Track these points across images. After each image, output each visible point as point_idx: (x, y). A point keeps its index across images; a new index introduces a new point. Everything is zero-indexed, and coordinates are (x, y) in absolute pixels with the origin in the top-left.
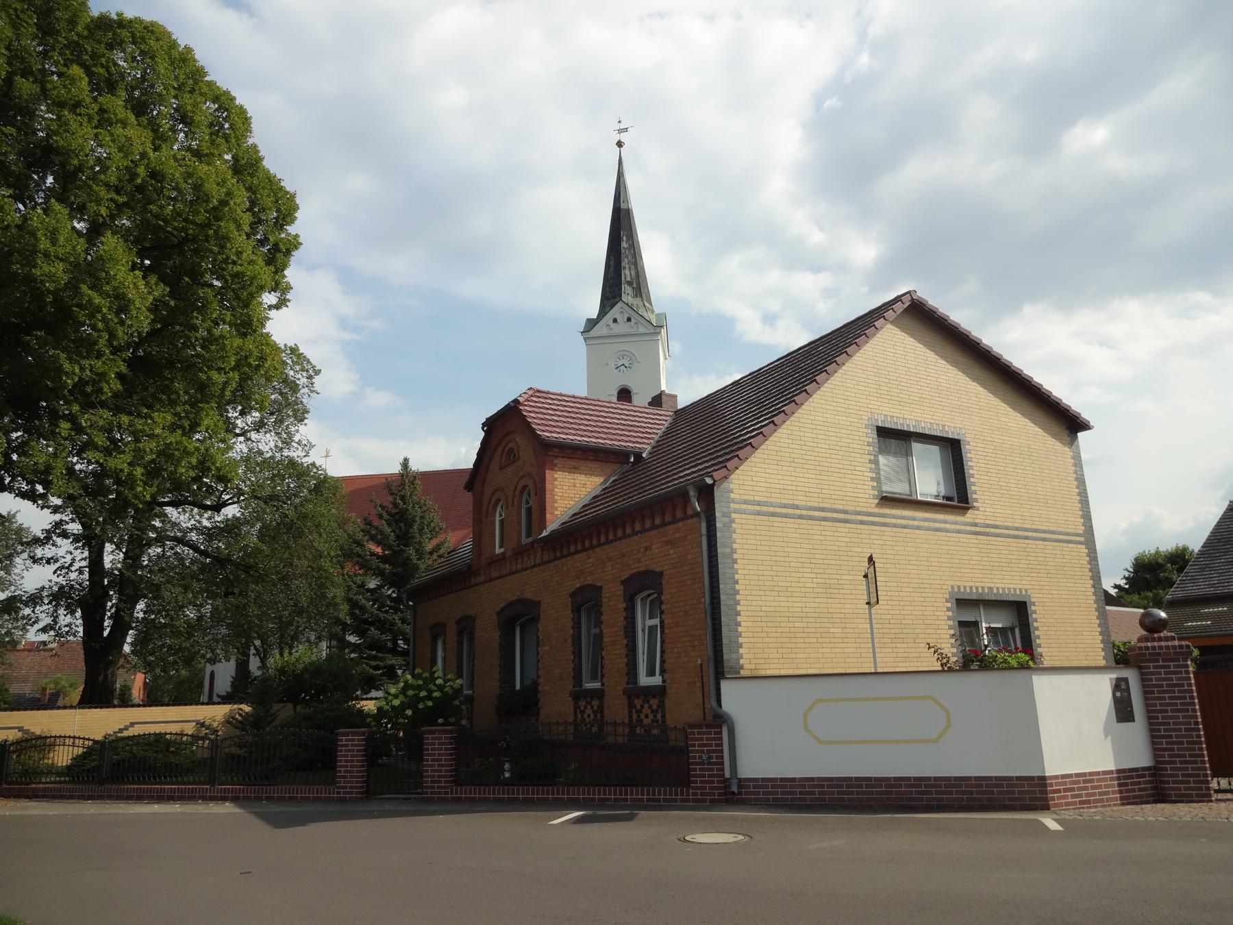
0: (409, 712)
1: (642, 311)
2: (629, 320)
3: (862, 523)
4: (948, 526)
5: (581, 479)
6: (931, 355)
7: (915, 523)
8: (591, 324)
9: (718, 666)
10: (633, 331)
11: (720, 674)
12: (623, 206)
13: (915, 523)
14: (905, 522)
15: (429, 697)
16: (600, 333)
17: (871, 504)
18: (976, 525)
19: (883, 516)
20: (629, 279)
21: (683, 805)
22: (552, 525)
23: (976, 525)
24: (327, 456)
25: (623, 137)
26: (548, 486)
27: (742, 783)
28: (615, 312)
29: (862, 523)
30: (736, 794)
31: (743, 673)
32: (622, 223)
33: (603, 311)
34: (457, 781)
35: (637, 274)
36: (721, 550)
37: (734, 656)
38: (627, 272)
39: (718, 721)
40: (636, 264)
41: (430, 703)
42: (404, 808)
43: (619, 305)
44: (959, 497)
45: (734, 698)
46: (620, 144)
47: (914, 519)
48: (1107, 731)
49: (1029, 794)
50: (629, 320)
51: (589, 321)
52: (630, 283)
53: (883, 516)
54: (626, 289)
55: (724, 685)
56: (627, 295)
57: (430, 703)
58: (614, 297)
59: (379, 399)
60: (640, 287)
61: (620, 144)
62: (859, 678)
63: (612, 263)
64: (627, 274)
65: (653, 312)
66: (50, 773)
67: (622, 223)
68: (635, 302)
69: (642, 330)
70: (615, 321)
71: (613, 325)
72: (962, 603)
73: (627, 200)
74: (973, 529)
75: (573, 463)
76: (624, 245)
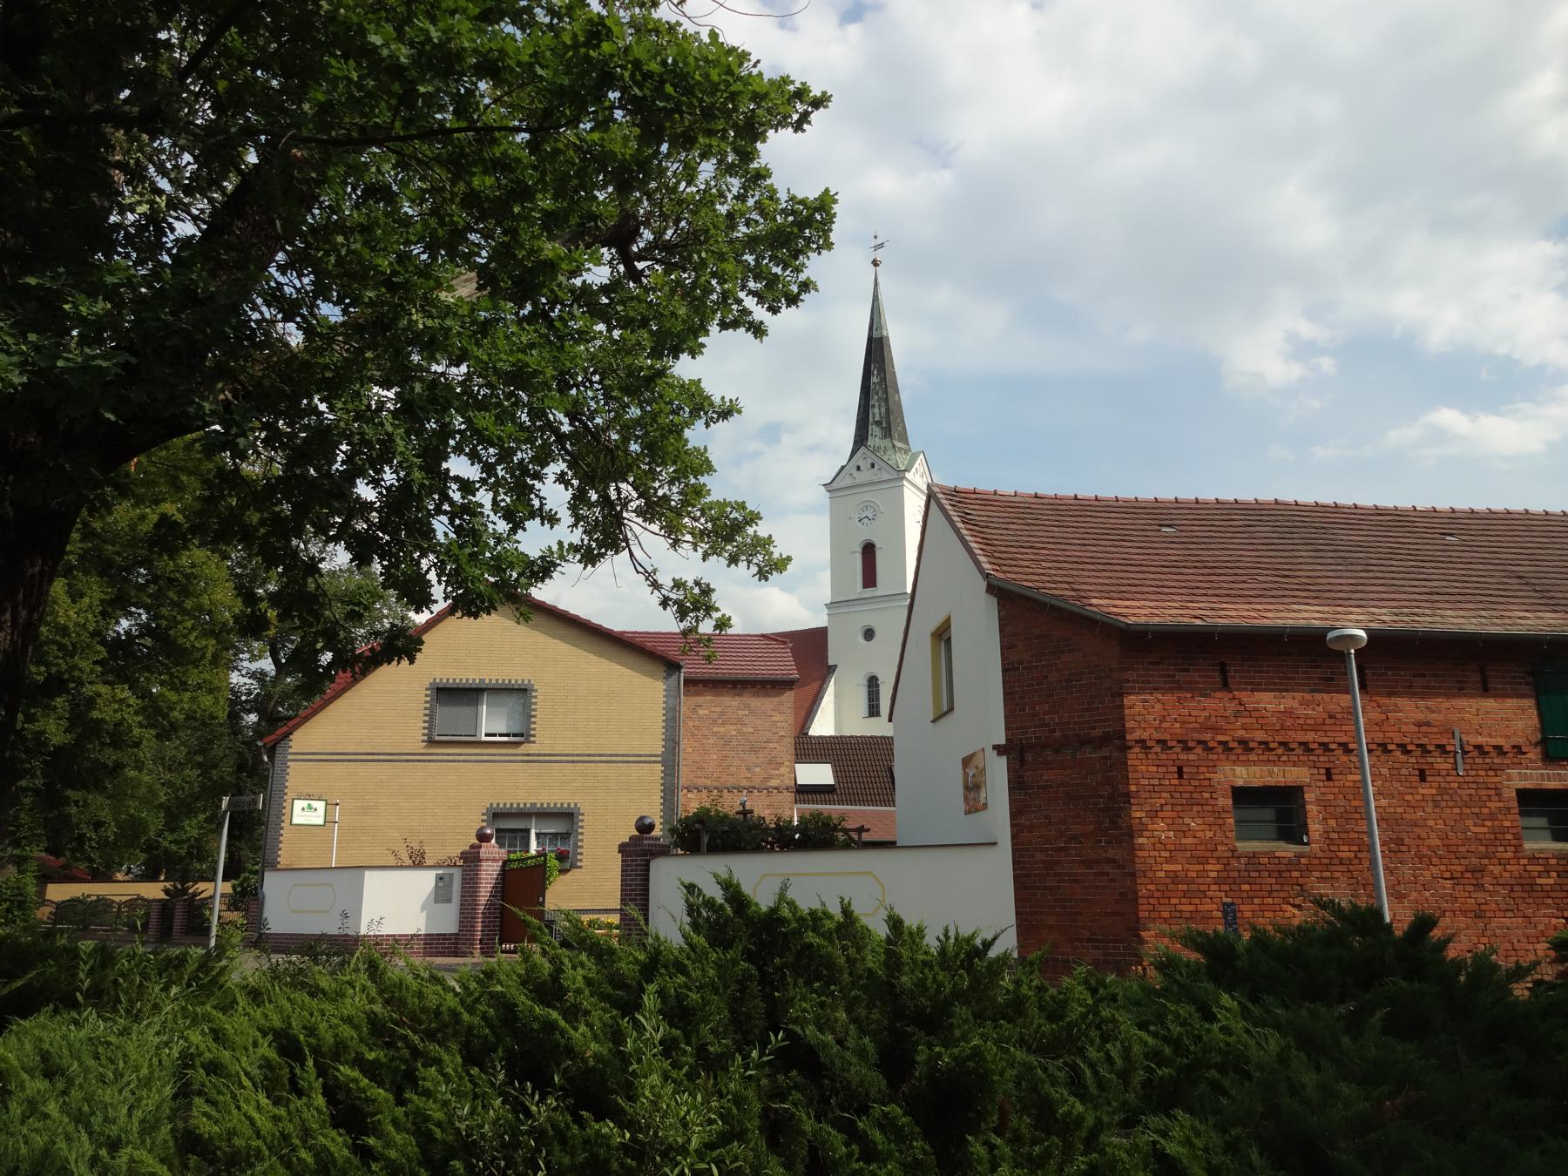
2: (873, 466)
10: (875, 479)
16: (842, 485)
17: (420, 747)
32: (877, 351)
34: (187, 933)
35: (888, 410)
38: (876, 411)
40: (886, 400)
44: (522, 736)
50: (873, 466)
52: (878, 423)
54: (874, 430)
61: (875, 263)
64: (876, 413)
67: (877, 351)
68: (886, 443)
69: (886, 476)
70: (858, 468)
73: (880, 328)
76: (874, 379)
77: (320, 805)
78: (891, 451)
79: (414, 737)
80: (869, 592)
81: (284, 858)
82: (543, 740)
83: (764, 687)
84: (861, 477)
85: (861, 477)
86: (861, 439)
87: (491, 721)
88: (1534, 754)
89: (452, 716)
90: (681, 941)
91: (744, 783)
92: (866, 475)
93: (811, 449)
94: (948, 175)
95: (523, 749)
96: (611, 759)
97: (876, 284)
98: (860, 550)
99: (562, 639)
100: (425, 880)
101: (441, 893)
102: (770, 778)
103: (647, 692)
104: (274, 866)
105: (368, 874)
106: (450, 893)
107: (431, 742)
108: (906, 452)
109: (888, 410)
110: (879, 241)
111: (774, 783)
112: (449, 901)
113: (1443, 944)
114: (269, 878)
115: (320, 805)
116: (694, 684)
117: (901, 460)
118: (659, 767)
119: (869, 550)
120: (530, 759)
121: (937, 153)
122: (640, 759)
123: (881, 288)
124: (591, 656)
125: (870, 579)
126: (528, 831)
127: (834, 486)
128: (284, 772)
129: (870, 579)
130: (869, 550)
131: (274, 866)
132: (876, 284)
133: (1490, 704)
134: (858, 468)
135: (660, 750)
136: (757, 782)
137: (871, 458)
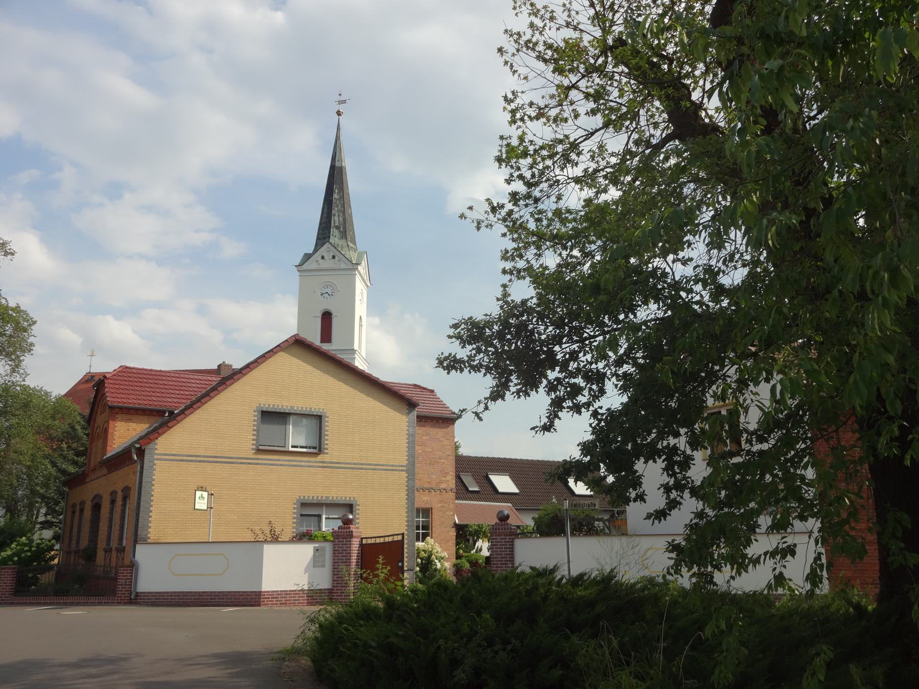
0: (16, 559)
2: (334, 257)
3: (242, 463)
4: (303, 464)
5: (133, 425)
6: (309, 368)
7: (279, 463)
8: (307, 257)
9: (136, 539)
10: (336, 267)
11: (136, 542)
13: (279, 463)
14: (272, 462)
15: (30, 551)
17: (250, 453)
18: (324, 462)
19: (258, 459)
20: (337, 224)
23: (324, 462)
24: (92, 356)
25: (342, 108)
26: (110, 430)
27: (137, 594)
28: (323, 251)
29: (242, 463)
30: (137, 600)
31: (149, 541)
32: (336, 176)
33: (316, 250)
34: (15, 595)
35: (344, 219)
36: (144, 479)
37: (144, 533)
38: (336, 218)
39: (133, 566)
40: (344, 212)
41: (29, 554)
43: (327, 245)
44: (318, 449)
45: (142, 554)
46: (339, 113)
47: (279, 460)
48: (306, 570)
49: (252, 599)
50: (334, 257)
51: (306, 254)
52: (337, 228)
53: (258, 459)
54: (334, 232)
55: (138, 547)
57: (29, 554)
58: (324, 238)
59: (231, 249)
60: (346, 231)
62: (167, 546)
63: (326, 210)
64: (336, 220)
65: (355, 250)
66: (52, 666)
67: (336, 176)
68: (342, 242)
69: (343, 266)
70: (323, 258)
71: (321, 261)
72: (304, 505)
73: (341, 160)
75: (129, 417)
76: (336, 196)
77: (198, 494)
78: (346, 249)
79: (245, 444)
81: (153, 533)
82: (334, 449)
83: (438, 422)
84: (324, 264)
85: (324, 264)
86: (323, 236)
87: (296, 436)
89: (273, 429)
90: (559, 577)
91: (426, 486)
92: (328, 263)
94: (279, 17)
95: (320, 458)
96: (376, 467)
97: (338, 129)
98: (320, 315)
99: (345, 382)
100: (307, 550)
101: (316, 561)
102: (442, 482)
103: (397, 423)
104: (145, 541)
105: (266, 546)
106: (324, 561)
108: (355, 250)
109: (344, 219)
110: (342, 98)
111: (443, 486)
112: (323, 566)
113: (326, 620)
115: (198, 494)
116: (423, 419)
117: (354, 257)
118: (404, 474)
119: (327, 317)
120: (325, 466)
122: (392, 469)
123: (342, 132)
124: (363, 396)
126: (319, 516)
127: (304, 267)
128: (152, 468)
130: (327, 317)
131: (145, 541)
132: (338, 129)
134: (323, 258)
135: (405, 463)
136: (433, 485)
137: (333, 252)
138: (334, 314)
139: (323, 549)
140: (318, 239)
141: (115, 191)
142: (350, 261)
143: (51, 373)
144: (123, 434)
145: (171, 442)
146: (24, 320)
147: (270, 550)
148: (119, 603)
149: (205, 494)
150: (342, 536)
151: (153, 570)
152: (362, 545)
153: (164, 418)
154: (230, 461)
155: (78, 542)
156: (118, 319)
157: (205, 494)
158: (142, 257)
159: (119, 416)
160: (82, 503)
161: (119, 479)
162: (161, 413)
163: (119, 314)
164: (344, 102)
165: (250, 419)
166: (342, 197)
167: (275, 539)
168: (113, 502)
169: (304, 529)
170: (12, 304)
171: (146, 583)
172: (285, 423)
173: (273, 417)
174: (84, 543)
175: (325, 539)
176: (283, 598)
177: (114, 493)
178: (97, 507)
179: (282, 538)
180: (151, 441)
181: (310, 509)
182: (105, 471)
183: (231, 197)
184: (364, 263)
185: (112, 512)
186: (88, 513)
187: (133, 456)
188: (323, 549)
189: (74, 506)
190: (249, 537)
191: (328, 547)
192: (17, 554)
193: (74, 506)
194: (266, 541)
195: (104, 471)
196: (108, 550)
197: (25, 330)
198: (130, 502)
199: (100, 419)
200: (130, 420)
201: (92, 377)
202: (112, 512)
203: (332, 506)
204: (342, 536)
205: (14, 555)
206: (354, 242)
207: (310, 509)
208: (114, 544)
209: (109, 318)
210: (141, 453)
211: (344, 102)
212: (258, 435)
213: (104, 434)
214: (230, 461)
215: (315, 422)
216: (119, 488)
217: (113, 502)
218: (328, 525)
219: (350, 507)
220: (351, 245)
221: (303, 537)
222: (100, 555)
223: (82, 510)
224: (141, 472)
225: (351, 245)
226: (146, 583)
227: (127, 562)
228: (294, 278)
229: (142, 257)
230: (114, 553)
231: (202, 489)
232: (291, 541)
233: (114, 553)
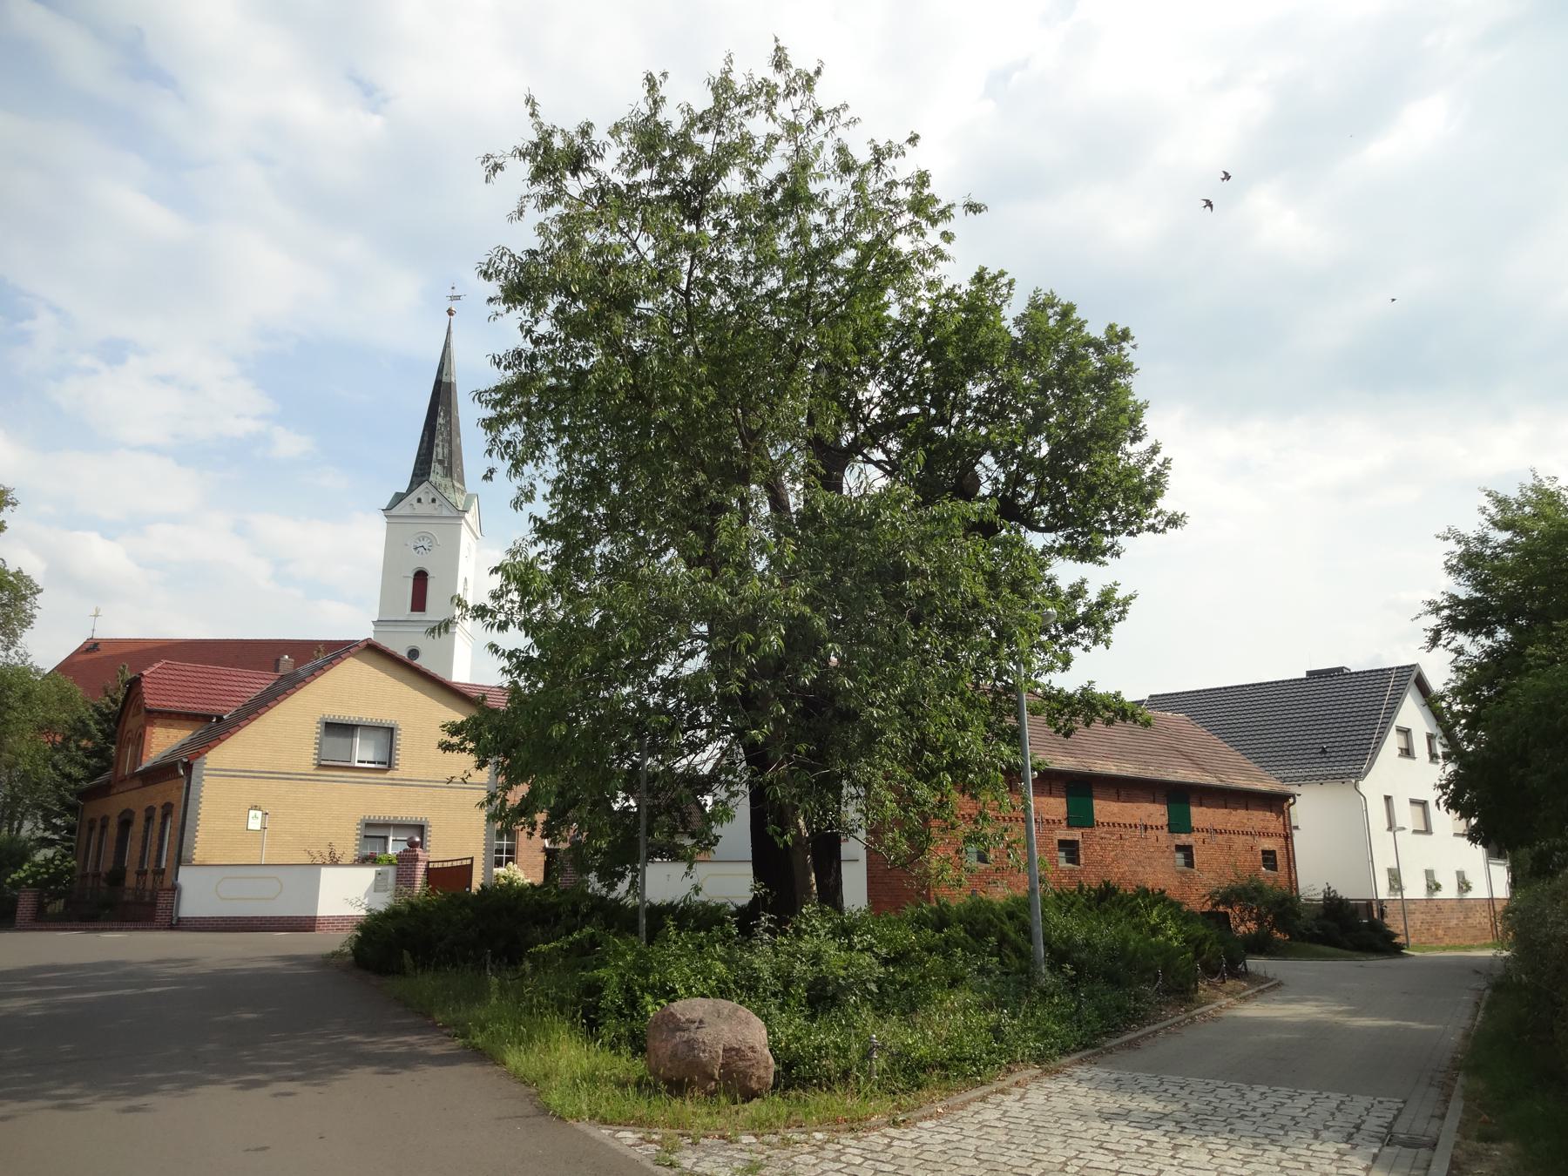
1: (449, 494)
2: (434, 501)
5: (173, 732)
6: (382, 675)
8: (399, 498)
9: (180, 860)
10: (436, 513)
11: (179, 863)
12: (445, 379)
16: (402, 513)
17: (311, 769)
21: (151, 929)
22: (146, 763)
25: (455, 306)
28: (420, 492)
33: (410, 490)
34: (36, 920)
35: (450, 452)
39: (175, 889)
40: (450, 442)
42: (436, 1050)
43: (426, 484)
44: (388, 764)
45: (185, 876)
49: (306, 924)
50: (434, 501)
52: (441, 462)
54: (436, 467)
55: (182, 870)
56: (437, 475)
59: (290, 444)
61: (450, 312)
64: (439, 451)
65: (463, 492)
68: (447, 481)
69: (445, 513)
70: (419, 500)
71: (416, 505)
72: (369, 825)
74: (98, 829)
76: (440, 420)
80: (417, 616)
87: (363, 751)
88: (1064, 823)
89: (337, 742)
93: (165, 380)
94: (376, 121)
95: (389, 774)
100: (368, 874)
101: (377, 886)
104: (189, 863)
105: (324, 870)
107: (320, 766)
108: (463, 492)
109: (450, 452)
114: (184, 873)
115: (252, 813)
117: (460, 500)
119: (421, 578)
120: (394, 783)
121: (370, 94)
125: (419, 603)
126: (386, 838)
127: (394, 512)
128: (200, 784)
129: (419, 603)
130: (421, 578)
131: (189, 863)
133: (1052, 800)
134: (419, 500)
138: (431, 574)
139: (386, 873)
140: (414, 475)
141: (114, 352)
142: (455, 507)
143: (45, 646)
144: (162, 742)
145: (219, 757)
146: (27, 586)
147: (327, 874)
148: (158, 929)
149: (259, 814)
150: (406, 861)
151: (197, 894)
152: (428, 870)
153: (213, 728)
154: (288, 777)
155: (97, 866)
156: (104, 536)
157: (259, 814)
158: (151, 449)
159: (158, 721)
160: (105, 820)
161: (157, 795)
162: (206, 718)
163: (109, 531)
164: (458, 298)
165: (312, 731)
166: (449, 422)
167: (335, 862)
168: (149, 819)
169: (368, 852)
170: (12, 568)
171: (190, 906)
172: (352, 736)
173: (338, 729)
174: (107, 865)
175: (390, 863)
176: (336, 922)
177: (150, 811)
178: (126, 823)
179: (343, 861)
180: (199, 755)
181: (375, 831)
182: (137, 783)
183: (293, 370)
184: (473, 509)
185: (146, 831)
186: (113, 829)
187: (177, 770)
188: (386, 873)
189: (92, 821)
190: (306, 859)
191: (391, 870)
192: (33, 876)
193: (92, 821)
194: (324, 864)
195: (137, 783)
196: (141, 873)
197: (24, 598)
198: (173, 818)
199: (132, 723)
200: (171, 726)
201: (96, 644)
202: (146, 831)
203: (400, 826)
204: (406, 861)
205: (27, 877)
206: (462, 482)
207: (375, 831)
208: (149, 866)
209: (94, 537)
210: (188, 767)
211: (458, 298)
212: (320, 749)
213: (139, 740)
214: (288, 777)
215: (382, 737)
216: (158, 804)
217: (149, 819)
218: (393, 849)
219: (421, 829)
220: (457, 485)
221: (366, 860)
222: (131, 880)
223: (104, 827)
224: (188, 788)
225: (457, 485)
226: (190, 906)
227: (167, 884)
228: (380, 522)
229: (151, 449)
230: (150, 876)
231: (255, 808)
232: (352, 865)
233: (150, 876)
